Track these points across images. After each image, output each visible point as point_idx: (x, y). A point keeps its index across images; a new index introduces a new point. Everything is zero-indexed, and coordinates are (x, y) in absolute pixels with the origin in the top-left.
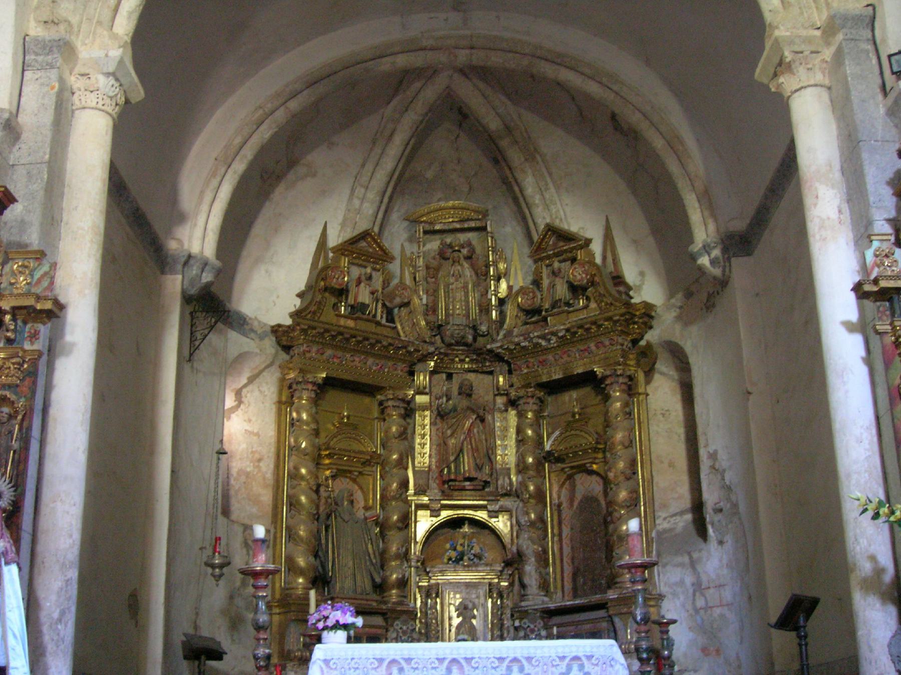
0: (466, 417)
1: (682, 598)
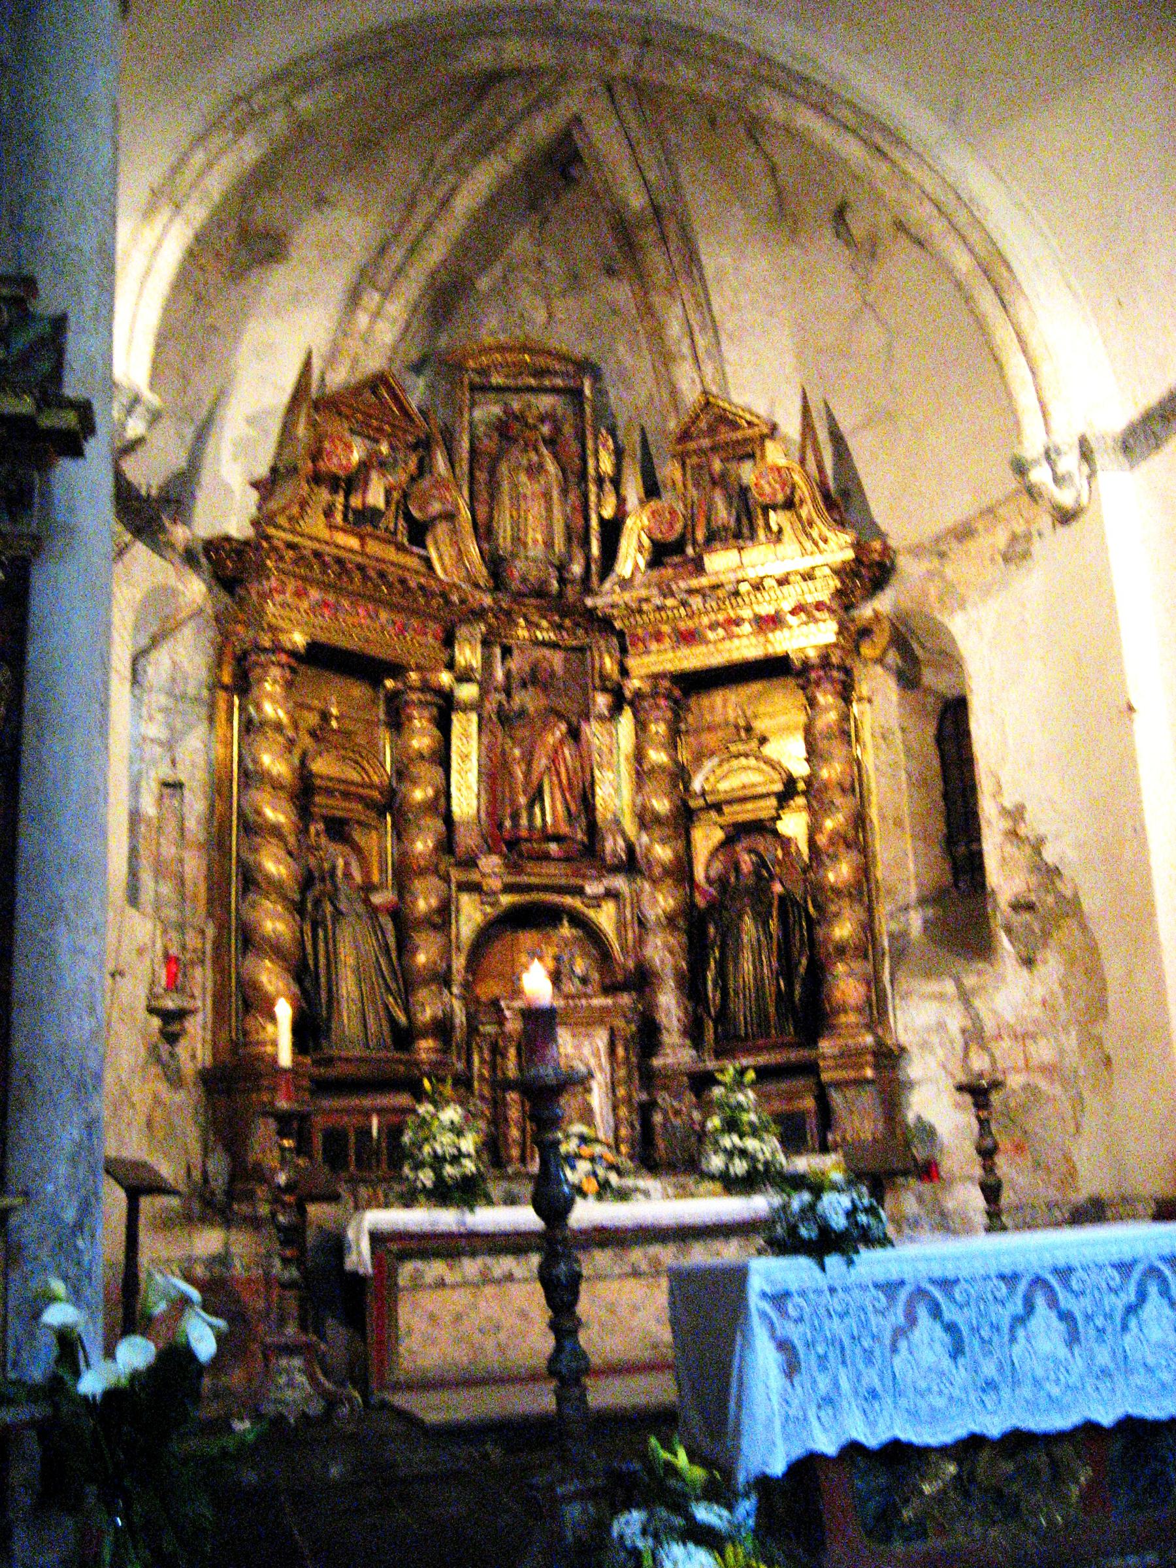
0: (546, 727)
1: (940, 1052)
